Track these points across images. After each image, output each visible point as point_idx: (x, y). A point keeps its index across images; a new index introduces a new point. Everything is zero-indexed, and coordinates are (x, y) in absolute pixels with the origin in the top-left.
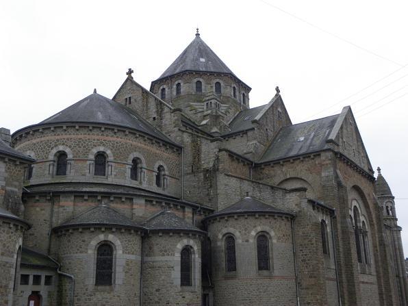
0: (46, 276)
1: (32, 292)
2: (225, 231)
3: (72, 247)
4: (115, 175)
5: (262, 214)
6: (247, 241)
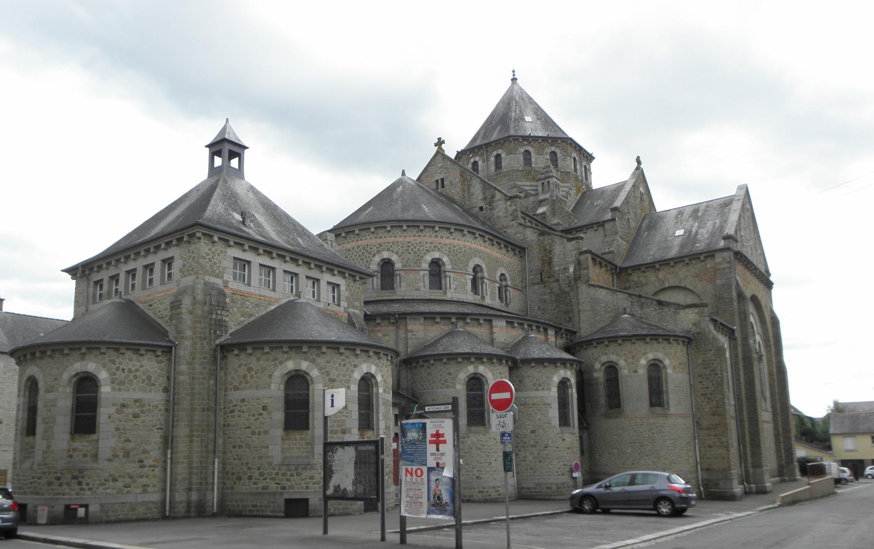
2: (604, 359)
3: (434, 381)
4: (455, 289)
5: (655, 338)
6: (635, 371)
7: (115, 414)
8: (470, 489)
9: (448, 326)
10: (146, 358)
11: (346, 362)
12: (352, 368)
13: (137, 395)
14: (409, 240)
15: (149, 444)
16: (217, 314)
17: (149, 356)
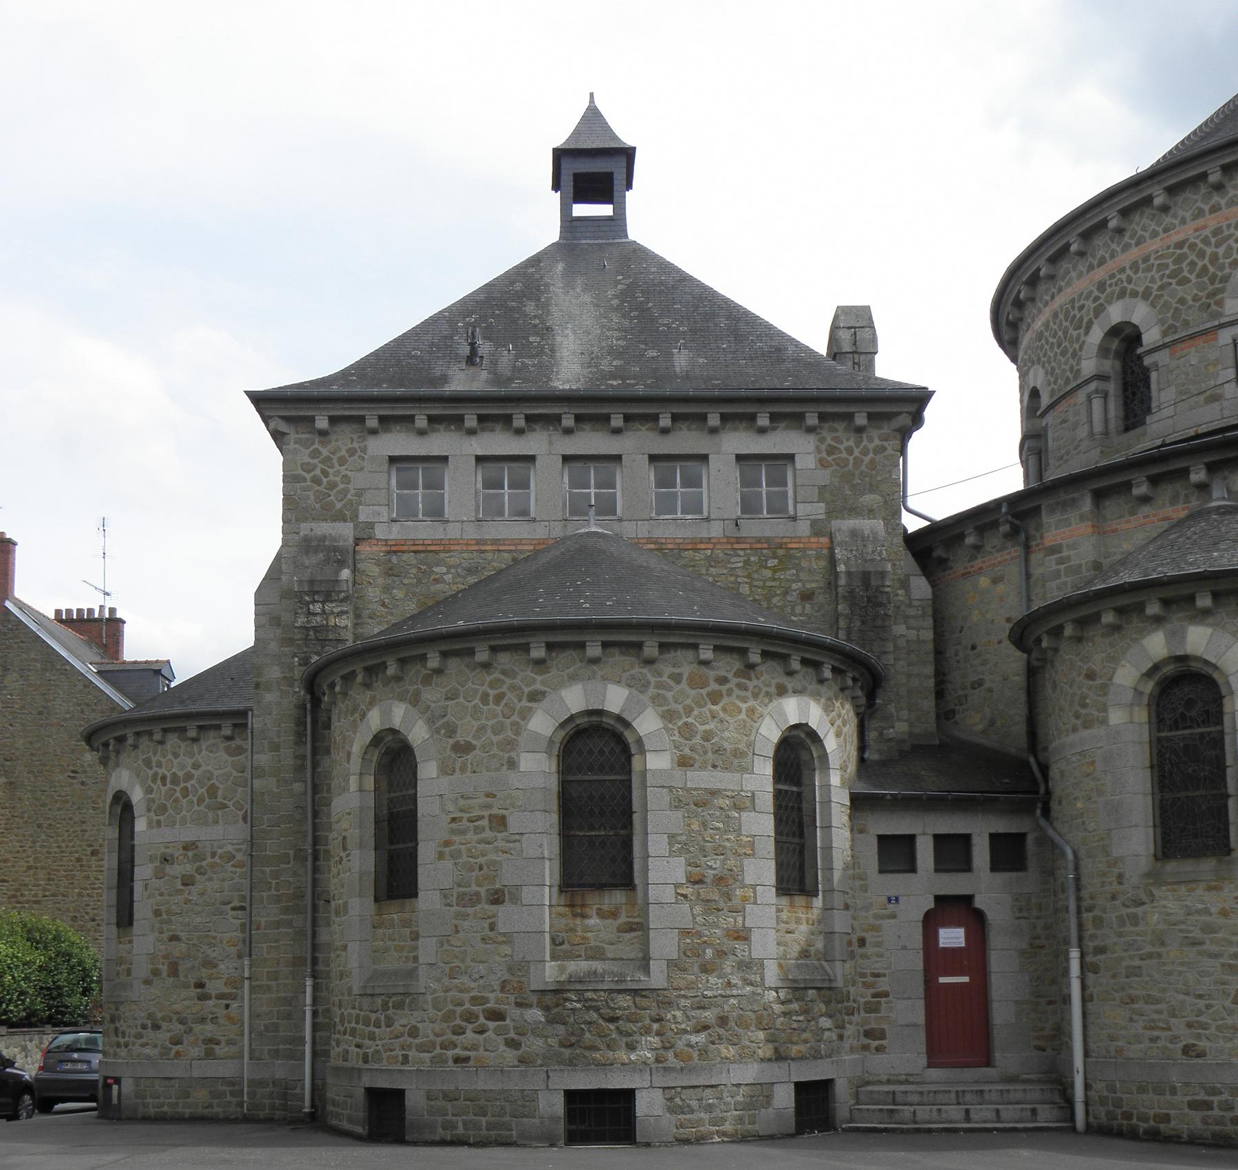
0: (994, 837)
1: (939, 899)
7: (154, 880)
8: (1159, 1091)
9: (1187, 501)
10: (204, 745)
11: (504, 689)
12: (525, 703)
13: (189, 833)
14: (1180, 237)
15: (215, 945)
16: (310, 614)
17: (211, 741)
